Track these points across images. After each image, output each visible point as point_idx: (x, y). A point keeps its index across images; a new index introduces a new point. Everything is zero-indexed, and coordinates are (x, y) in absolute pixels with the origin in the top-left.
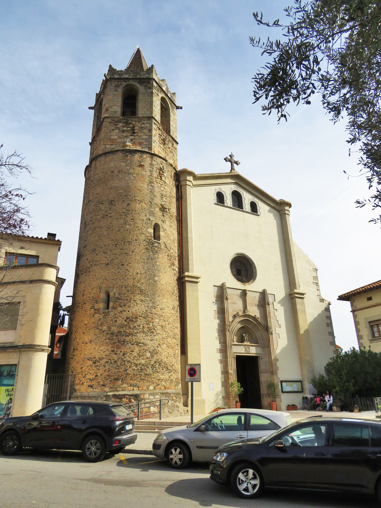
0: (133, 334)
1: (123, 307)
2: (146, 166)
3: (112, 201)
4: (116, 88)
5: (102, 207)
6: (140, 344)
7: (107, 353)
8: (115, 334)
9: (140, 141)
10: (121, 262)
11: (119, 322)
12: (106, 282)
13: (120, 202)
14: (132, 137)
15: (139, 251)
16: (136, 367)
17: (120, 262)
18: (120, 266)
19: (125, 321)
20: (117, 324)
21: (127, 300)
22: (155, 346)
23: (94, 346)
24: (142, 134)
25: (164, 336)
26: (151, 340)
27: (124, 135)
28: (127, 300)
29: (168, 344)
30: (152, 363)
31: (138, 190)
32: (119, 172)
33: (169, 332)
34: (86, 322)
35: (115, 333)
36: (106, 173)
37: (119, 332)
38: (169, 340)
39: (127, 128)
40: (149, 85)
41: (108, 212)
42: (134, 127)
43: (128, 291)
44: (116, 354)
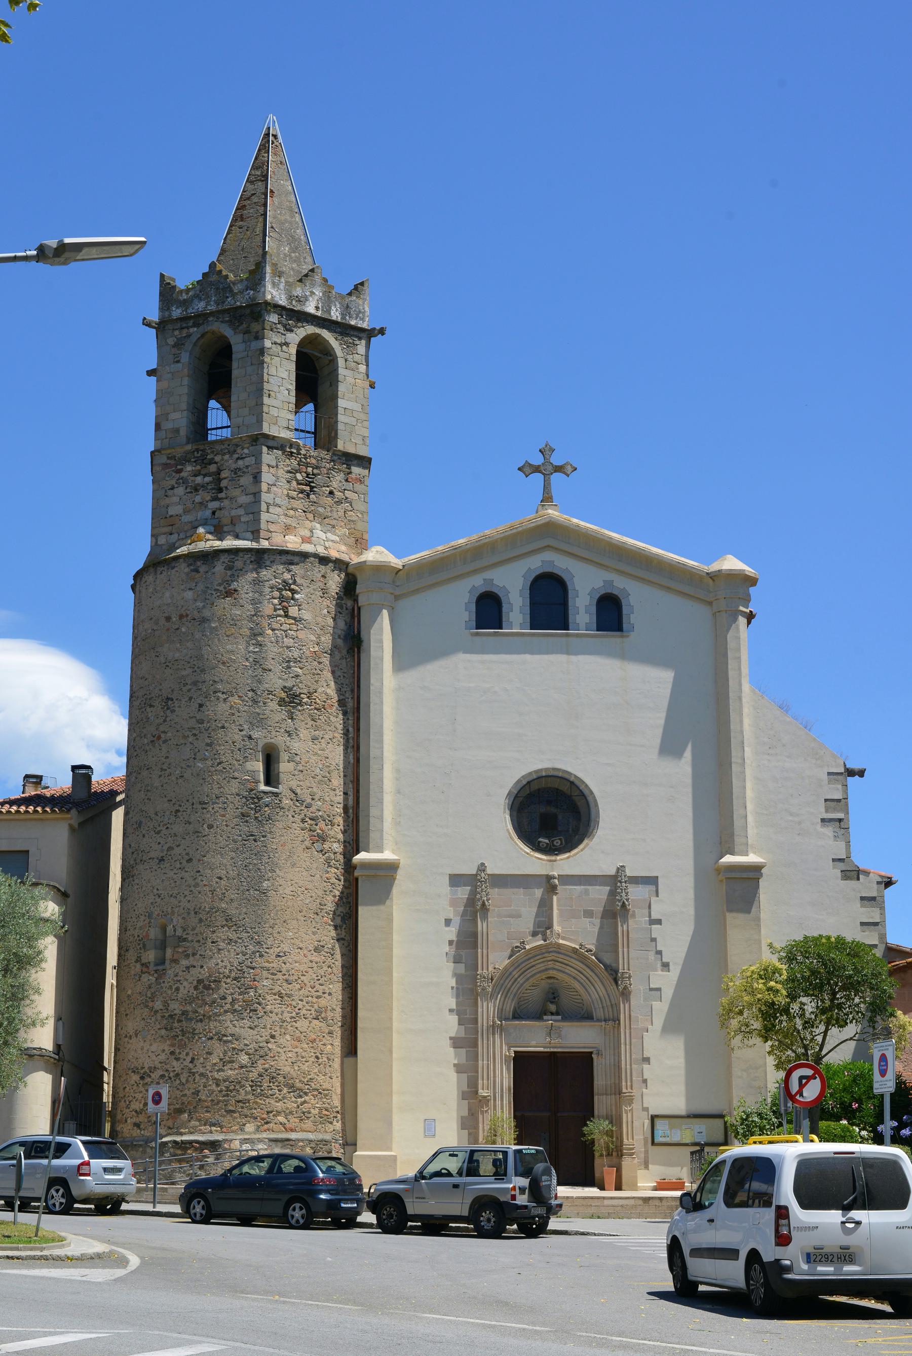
0: (210, 1016)
1: (191, 958)
3: (168, 699)
4: (174, 351)
5: (151, 713)
6: (225, 1038)
7: (163, 1057)
9: (233, 513)
11: (183, 992)
12: (158, 900)
14: (214, 505)
15: (226, 821)
16: (218, 1085)
17: (184, 853)
18: (184, 862)
19: (196, 988)
20: (180, 995)
21: (199, 941)
22: (260, 1039)
23: (142, 1044)
24: (236, 492)
25: (287, 1016)
26: (251, 1028)
28: (199, 941)
29: (298, 1034)
30: (253, 1075)
31: (224, 663)
33: (300, 1006)
34: (129, 992)
37: (184, 1013)
38: (302, 1024)
39: (205, 476)
40: (255, 327)
41: (162, 728)
43: (201, 920)
44: (177, 1059)
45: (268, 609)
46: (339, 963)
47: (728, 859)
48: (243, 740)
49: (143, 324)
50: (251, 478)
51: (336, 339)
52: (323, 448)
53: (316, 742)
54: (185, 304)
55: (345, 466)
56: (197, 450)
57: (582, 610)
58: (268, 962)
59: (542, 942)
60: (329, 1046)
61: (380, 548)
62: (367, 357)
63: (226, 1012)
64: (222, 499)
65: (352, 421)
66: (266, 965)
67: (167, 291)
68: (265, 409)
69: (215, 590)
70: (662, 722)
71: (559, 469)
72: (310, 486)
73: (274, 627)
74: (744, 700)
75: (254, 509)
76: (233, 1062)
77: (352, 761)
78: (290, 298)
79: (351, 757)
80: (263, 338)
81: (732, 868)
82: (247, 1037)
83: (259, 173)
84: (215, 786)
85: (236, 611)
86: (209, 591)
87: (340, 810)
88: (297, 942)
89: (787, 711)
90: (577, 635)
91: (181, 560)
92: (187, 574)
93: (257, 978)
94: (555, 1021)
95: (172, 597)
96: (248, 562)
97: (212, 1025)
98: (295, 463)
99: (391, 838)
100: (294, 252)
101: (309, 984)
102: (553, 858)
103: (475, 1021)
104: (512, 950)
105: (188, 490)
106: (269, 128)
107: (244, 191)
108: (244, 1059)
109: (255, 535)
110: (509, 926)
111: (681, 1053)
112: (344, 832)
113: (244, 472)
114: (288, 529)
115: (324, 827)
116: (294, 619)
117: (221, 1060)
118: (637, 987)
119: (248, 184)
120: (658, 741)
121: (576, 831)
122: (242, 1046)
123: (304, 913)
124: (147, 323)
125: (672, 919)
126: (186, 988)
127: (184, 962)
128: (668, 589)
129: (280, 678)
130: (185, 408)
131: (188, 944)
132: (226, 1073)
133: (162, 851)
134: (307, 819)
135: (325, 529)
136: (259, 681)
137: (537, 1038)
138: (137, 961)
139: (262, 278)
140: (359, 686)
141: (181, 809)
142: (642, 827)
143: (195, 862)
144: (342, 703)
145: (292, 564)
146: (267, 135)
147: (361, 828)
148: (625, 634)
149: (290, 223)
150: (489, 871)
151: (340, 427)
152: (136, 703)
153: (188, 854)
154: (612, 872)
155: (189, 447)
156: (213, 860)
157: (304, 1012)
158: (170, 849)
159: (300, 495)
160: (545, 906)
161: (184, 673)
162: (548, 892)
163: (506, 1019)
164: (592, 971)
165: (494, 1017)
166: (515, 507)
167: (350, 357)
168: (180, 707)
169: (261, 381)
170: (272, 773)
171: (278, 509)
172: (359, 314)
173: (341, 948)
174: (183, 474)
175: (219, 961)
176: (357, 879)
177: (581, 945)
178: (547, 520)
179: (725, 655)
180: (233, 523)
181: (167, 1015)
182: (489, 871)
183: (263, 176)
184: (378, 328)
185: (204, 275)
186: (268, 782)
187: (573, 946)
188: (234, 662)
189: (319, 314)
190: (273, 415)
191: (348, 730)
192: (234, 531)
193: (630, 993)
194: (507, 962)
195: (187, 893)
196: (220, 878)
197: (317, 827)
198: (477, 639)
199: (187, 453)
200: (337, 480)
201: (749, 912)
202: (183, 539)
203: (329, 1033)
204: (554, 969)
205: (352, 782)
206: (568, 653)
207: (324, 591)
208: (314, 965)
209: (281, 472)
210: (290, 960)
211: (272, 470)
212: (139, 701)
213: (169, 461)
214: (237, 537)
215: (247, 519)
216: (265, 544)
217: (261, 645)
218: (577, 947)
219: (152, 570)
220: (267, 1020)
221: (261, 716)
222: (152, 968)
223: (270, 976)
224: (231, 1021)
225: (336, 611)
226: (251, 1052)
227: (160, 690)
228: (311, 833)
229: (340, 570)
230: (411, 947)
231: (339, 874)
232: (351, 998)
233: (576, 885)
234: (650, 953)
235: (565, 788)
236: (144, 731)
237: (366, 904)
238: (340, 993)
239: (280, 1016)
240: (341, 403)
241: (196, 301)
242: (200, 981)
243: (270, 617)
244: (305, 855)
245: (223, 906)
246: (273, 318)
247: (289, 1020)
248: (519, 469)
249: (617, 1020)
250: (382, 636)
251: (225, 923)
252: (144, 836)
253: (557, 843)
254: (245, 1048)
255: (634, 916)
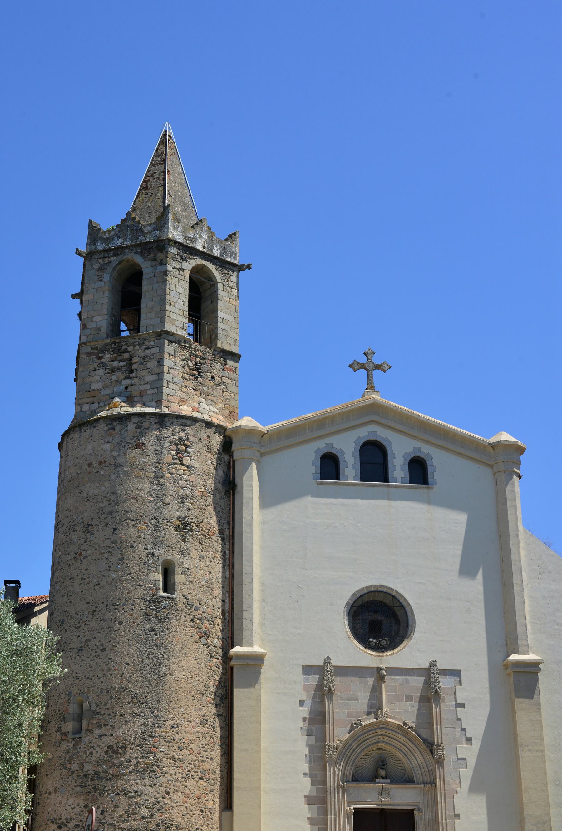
1: (103, 728)
2: (148, 445)
3: (88, 525)
4: (99, 273)
5: (74, 536)
6: (129, 794)
7: (78, 810)
8: (90, 777)
9: (142, 388)
10: (102, 645)
11: (96, 756)
13: (101, 526)
14: (128, 382)
15: (133, 618)
17: (99, 644)
18: (99, 651)
19: (106, 753)
20: (93, 758)
21: (109, 715)
22: (158, 795)
24: (145, 373)
25: (179, 777)
26: (151, 786)
27: (114, 378)
28: (109, 715)
29: (188, 792)
31: (133, 498)
32: (100, 463)
33: (189, 769)
35: (89, 774)
36: (80, 468)
37: (97, 773)
38: (191, 783)
39: (120, 361)
40: (160, 256)
41: (83, 547)
42: (131, 358)
43: (111, 698)
45: (167, 458)
46: (218, 734)
47: (514, 657)
48: (147, 556)
49: (76, 253)
50: (156, 363)
51: (217, 269)
52: (206, 345)
53: (202, 560)
54: (108, 240)
55: (222, 359)
56: (115, 343)
57: (398, 468)
58: (165, 732)
59: (374, 720)
60: (211, 802)
61: (249, 418)
62: (238, 284)
63: (131, 772)
64: (133, 377)
65: (228, 328)
66: (163, 734)
67: (94, 232)
68: (167, 313)
69: (127, 443)
70: (460, 552)
71: (378, 367)
72: (198, 371)
73: (172, 471)
74: (520, 537)
75: (158, 385)
76: (135, 814)
77: (228, 576)
78: (185, 238)
79: (227, 573)
80: (166, 264)
81: (518, 664)
82: (147, 793)
83: (159, 159)
84: (125, 592)
85: (144, 458)
86: (123, 444)
87: (219, 614)
88: (187, 716)
89: (549, 547)
90: (395, 487)
91: (101, 421)
92: (106, 431)
93: (156, 745)
94: (384, 783)
95: (93, 449)
96: (153, 423)
97: (119, 783)
98: (188, 354)
99: (258, 636)
100: (185, 212)
101: (196, 751)
102: (381, 654)
103: (325, 783)
104: (351, 726)
105: (107, 371)
106: (166, 131)
107: (148, 171)
108: (145, 811)
109: (159, 403)
110: (349, 706)
111: (483, 811)
112: (222, 631)
113: (150, 359)
114: (182, 401)
115: (208, 626)
116: (187, 466)
117: (126, 812)
118: (449, 757)
119: (151, 166)
120: (458, 566)
121: (397, 633)
122: (143, 801)
123: (193, 693)
124: (78, 253)
125: (472, 703)
126: (98, 753)
127: (97, 732)
128: (460, 455)
129: (176, 510)
130: (106, 313)
131: (101, 717)
132: (129, 823)
133: (81, 643)
134: (195, 619)
135: (208, 403)
136: (161, 512)
137: (372, 797)
138: (57, 731)
139: (166, 223)
140: (234, 519)
141: (97, 610)
142: (447, 632)
143: (108, 650)
144: (221, 531)
145: (186, 426)
146: (165, 135)
147: (236, 627)
148: (430, 486)
149: (182, 192)
150: (333, 663)
151: (219, 331)
152: (62, 529)
153: (102, 645)
154: (427, 666)
155: (108, 341)
156: (122, 650)
157: (192, 773)
158: (87, 641)
159: (191, 377)
160: (376, 692)
161: (102, 505)
162: (378, 681)
163: (346, 782)
164: (413, 743)
165: (338, 780)
166: (349, 393)
167: (226, 283)
168: (98, 531)
169: (164, 294)
170: (169, 583)
171: (175, 385)
172: (232, 254)
173: (220, 722)
174: (103, 360)
175: (126, 731)
176: (232, 668)
177: (404, 722)
178: (373, 401)
179: (505, 504)
180: (141, 395)
181: (82, 775)
182: (333, 663)
183: (162, 161)
184: (246, 264)
185: (122, 220)
186: (165, 590)
187: (399, 723)
188: (142, 496)
189: (205, 251)
190: (172, 319)
191: (225, 553)
192: (142, 401)
193: (443, 761)
194: (348, 735)
195: (100, 675)
196: (128, 664)
197: (203, 626)
198: (321, 487)
199: (107, 345)
200: (217, 369)
201: (532, 698)
202: (102, 407)
203: (211, 791)
204: (383, 742)
205: (228, 592)
206: (389, 499)
207: (209, 447)
208: (200, 735)
209: (178, 360)
210: (182, 731)
211: (171, 357)
212: (64, 527)
213: (92, 351)
214: (144, 405)
215: (153, 392)
216: (165, 410)
217: (162, 485)
218: (402, 724)
219: (77, 429)
220: (164, 780)
221: (162, 539)
222: (70, 736)
223: (166, 744)
224: (135, 780)
225: (217, 463)
226: (150, 805)
227: (82, 518)
228: (198, 630)
229: (220, 433)
230: (275, 721)
231: (218, 663)
232: (227, 763)
233: (399, 675)
234: (457, 730)
235: (388, 601)
236: (69, 550)
237: (238, 687)
238: (219, 758)
239: (173, 776)
240: (220, 314)
241: (116, 239)
242: (110, 747)
243: (169, 464)
244: (193, 648)
245: (130, 686)
246: (174, 250)
247: (180, 780)
248: (350, 366)
249: (433, 783)
250: (251, 482)
251: (131, 700)
252: (66, 631)
253: (383, 643)
254: (146, 802)
255: (444, 701)
